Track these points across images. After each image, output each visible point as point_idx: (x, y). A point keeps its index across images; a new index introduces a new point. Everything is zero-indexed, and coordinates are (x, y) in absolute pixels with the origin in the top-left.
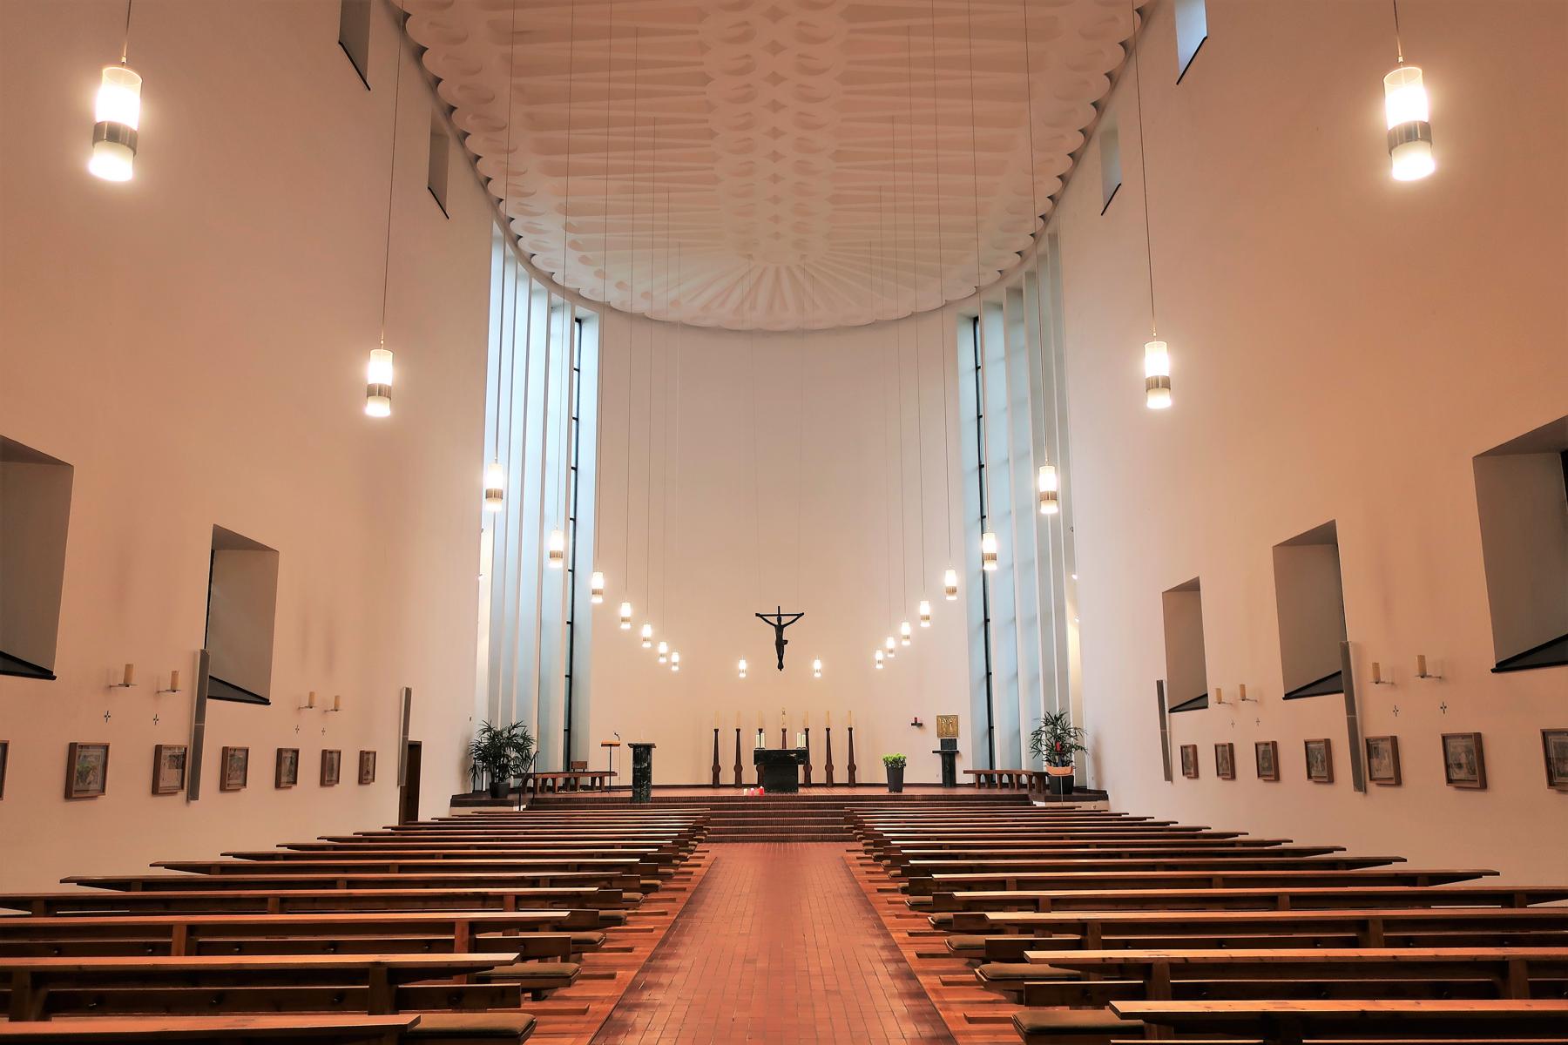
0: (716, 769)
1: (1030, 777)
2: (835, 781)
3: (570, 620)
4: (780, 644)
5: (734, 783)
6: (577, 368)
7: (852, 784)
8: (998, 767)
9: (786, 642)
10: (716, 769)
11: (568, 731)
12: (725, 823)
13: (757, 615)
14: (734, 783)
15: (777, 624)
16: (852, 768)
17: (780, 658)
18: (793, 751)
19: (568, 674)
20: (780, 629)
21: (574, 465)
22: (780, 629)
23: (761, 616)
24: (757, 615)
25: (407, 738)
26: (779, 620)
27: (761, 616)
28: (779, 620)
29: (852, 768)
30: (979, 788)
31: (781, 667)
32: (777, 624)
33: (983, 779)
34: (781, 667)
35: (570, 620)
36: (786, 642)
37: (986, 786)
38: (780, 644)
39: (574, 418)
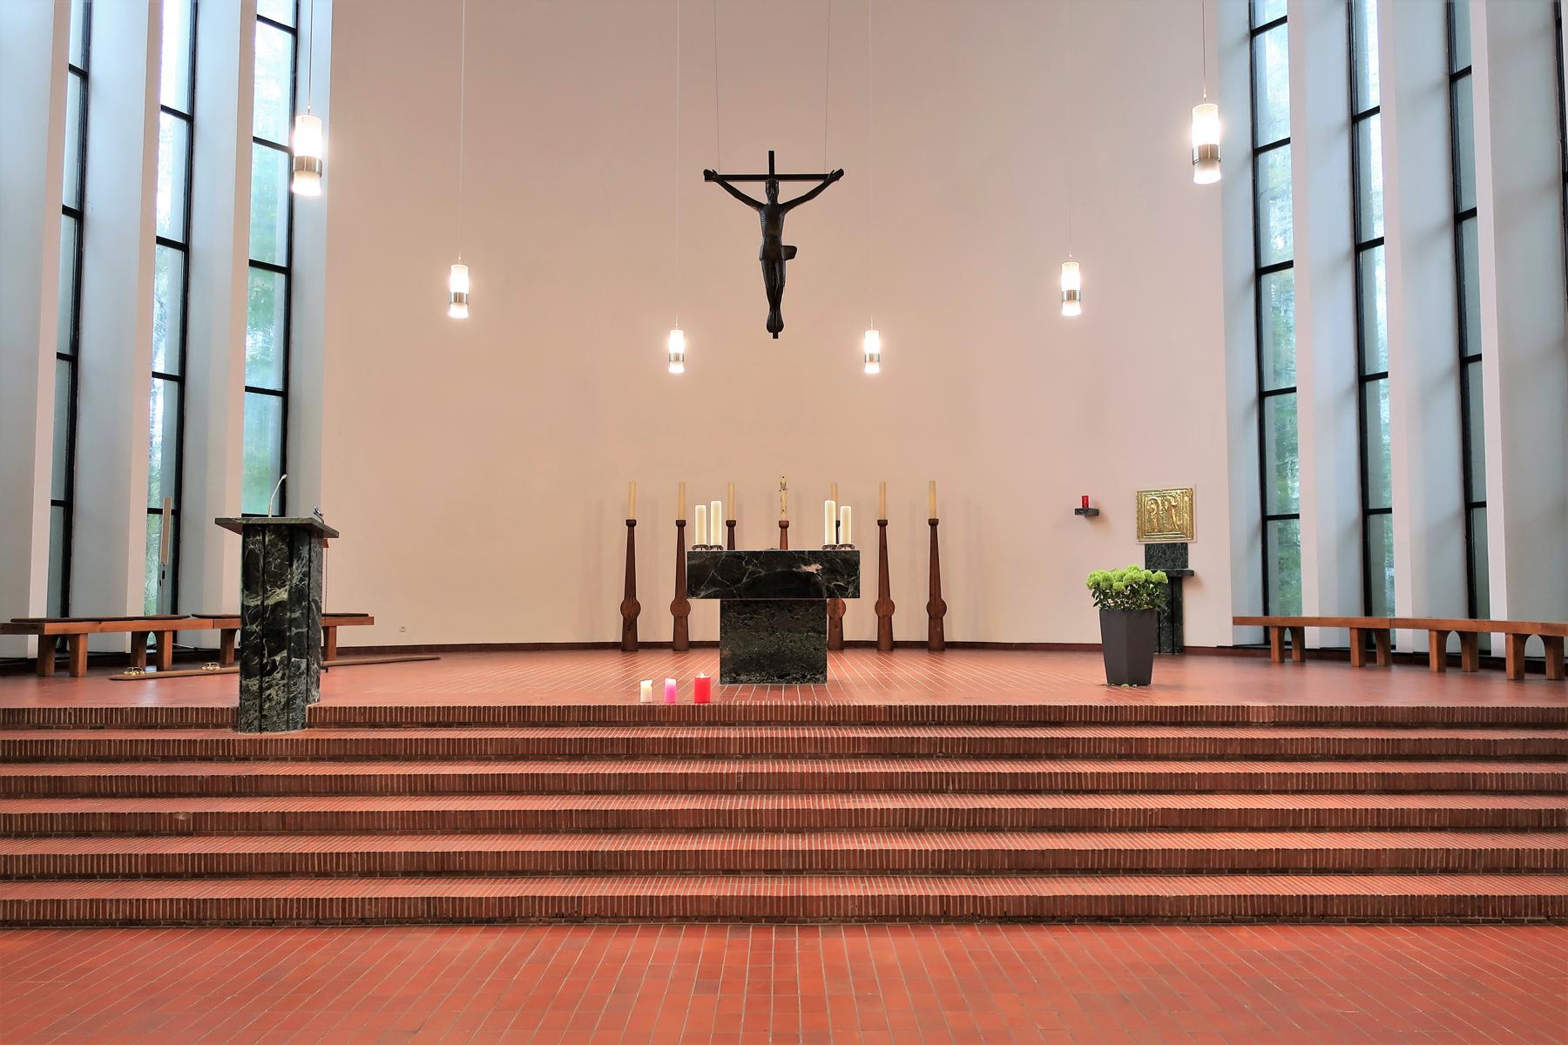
0: (630, 610)
1: (1519, 639)
2: (898, 636)
3: (66, 351)
4: (775, 257)
5: (620, 640)
6: (78, 64)
7: (936, 644)
8: (1499, 609)
9: (791, 252)
10: (630, 610)
11: (66, 505)
12: (755, 824)
13: (710, 176)
14: (620, 640)
15: (764, 200)
16: (937, 609)
17: (775, 294)
18: (814, 556)
19: (61, 498)
20: (773, 215)
21: (75, 59)
22: (773, 215)
23: (723, 180)
24: (710, 176)
25: (1284, 638)
26: (773, 192)
27: (723, 180)
28: (773, 192)
29: (937, 609)
30: (1518, 678)
31: (775, 326)
32: (764, 200)
33: (1453, 644)
34: (775, 326)
35: (66, 351)
36: (791, 252)
37: (1355, 656)
38: (775, 257)
39: (72, 68)
